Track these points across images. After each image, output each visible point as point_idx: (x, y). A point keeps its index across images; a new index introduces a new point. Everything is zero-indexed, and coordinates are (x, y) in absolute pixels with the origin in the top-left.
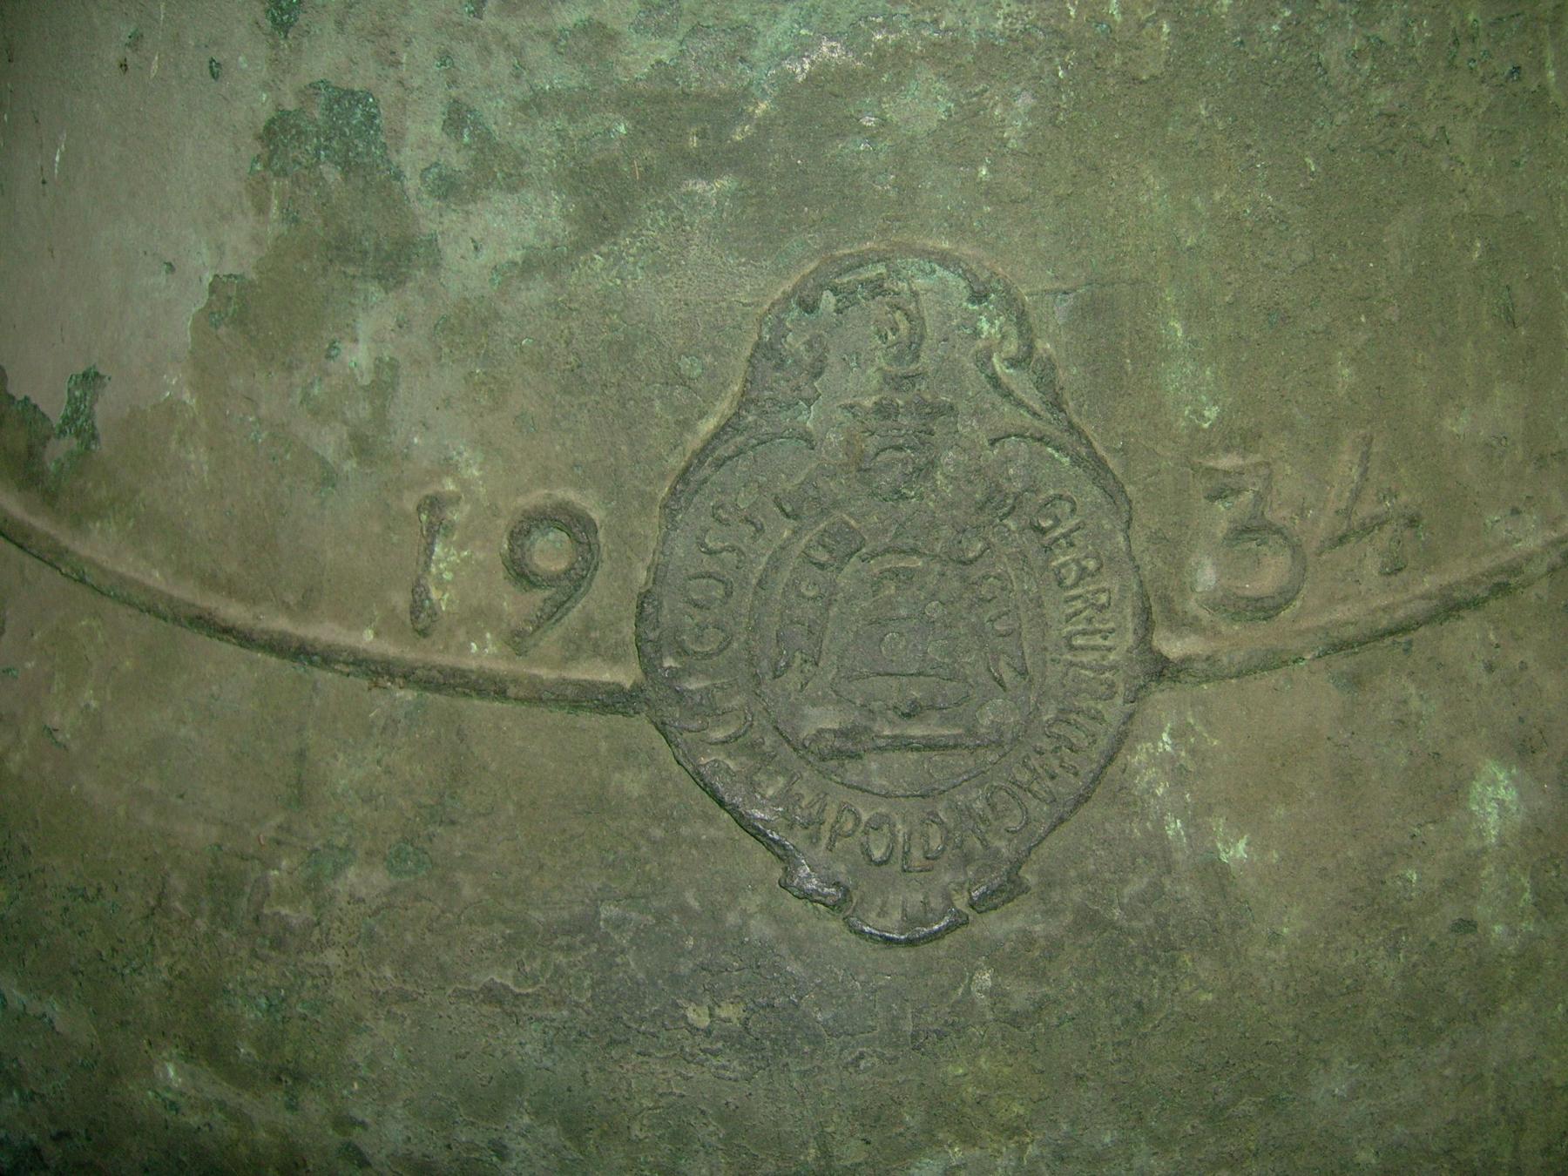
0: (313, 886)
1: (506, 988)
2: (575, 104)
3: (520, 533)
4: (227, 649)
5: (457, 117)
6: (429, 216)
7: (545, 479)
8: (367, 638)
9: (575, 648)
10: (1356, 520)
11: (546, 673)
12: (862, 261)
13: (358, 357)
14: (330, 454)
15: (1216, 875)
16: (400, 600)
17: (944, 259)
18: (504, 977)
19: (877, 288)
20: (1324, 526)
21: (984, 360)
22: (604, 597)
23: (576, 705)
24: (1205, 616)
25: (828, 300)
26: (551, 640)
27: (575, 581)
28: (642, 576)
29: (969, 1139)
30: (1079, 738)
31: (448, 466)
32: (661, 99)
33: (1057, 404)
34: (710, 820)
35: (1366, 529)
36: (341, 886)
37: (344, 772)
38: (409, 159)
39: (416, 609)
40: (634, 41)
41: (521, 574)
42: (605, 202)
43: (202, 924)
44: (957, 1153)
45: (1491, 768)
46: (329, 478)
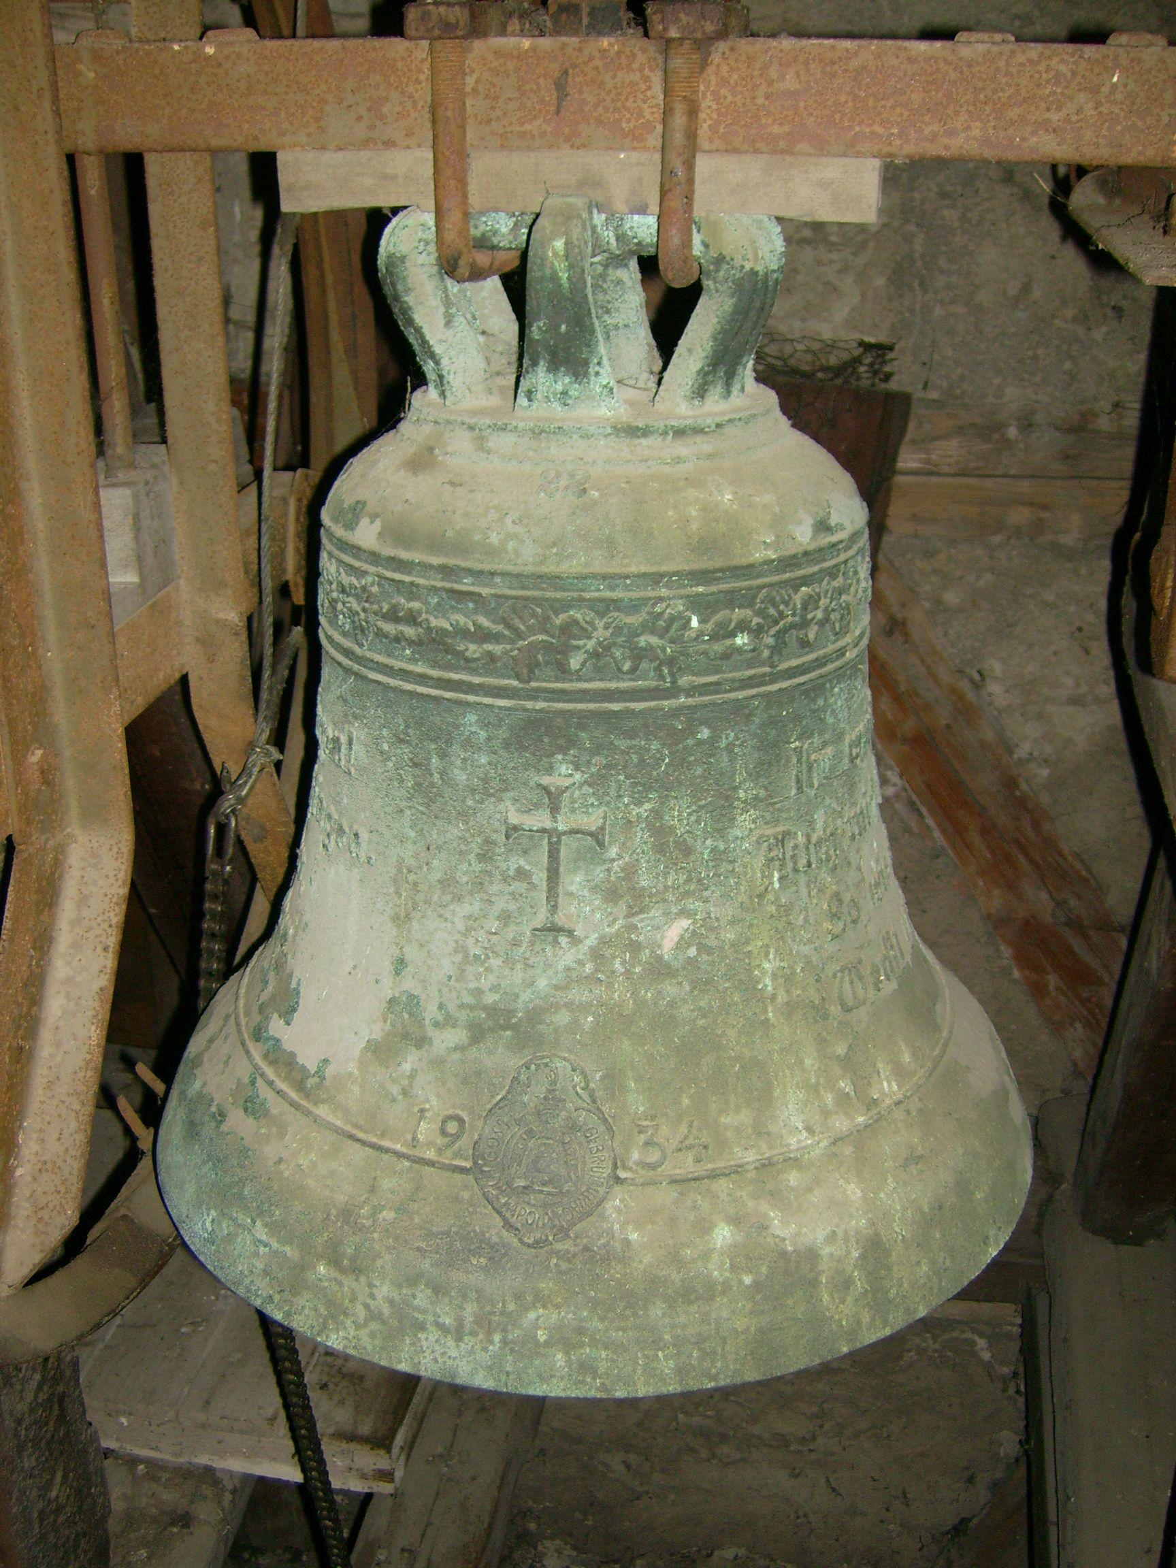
0: (373, 1215)
1: (436, 617)
2: (472, 1008)
3: (444, 1122)
4: (357, 1146)
5: (441, 1006)
6: (431, 1031)
7: (453, 1107)
8: (398, 1147)
9: (457, 1155)
10: (684, 1145)
11: (447, 1162)
12: (543, 1057)
13: (407, 1067)
14: (395, 1093)
15: (627, 1243)
16: (409, 1137)
17: (565, 1059)
18: (423, 1245)
19: (546, 1065)
20: (674, 1144)
21: (574, 1087)
22: (465, 1142)
23: (453, 1171)
24: (634, 1168)
25: (533, 1067)
26: (449, 1153)
27: (457, 1136)
28: (476, 1137)
29: (544, 1307)
30: (591, 1197)
31: (427, 1101)
32: (494, 1009)
33: (594, 1101)
34: (485, 1207)
35: (690, 1148)
36: (381, 1216)
37: (387, 1184)
38: (428, 1016)
39: (414, 1139)
40: (488, 993)
41: (444, 1133)
42: (477, 1033)
43: (339, 1224)
44: (541, 1311)
45: (722, 1225)
46: (394, 1100)
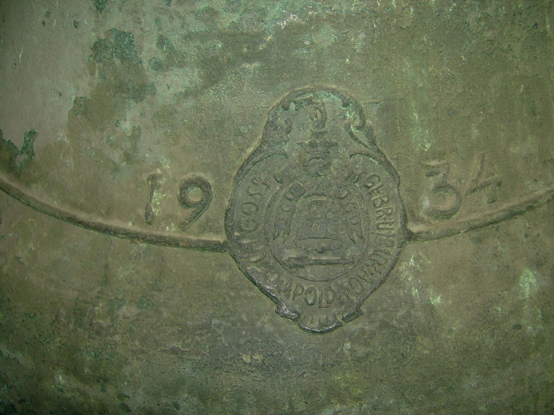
0: (110, 313)
2: (203, 37)
3: (184, 188)
4: (80, 229)
5: (162, 41)
6: (152, 76)
7: (193, 169)
8: (130, 225)
9: (203, 229)
10: (479, 184)
11: (193, 238)
12: (305, 92)
13: (127, 126)
14: (117, 160)
15: (430, 309)
16: (141, 212)
17: (334, 91)
18: (178, 345)
19: (310, 102)
20: (468, 186)
21: (348, 127)
22: (214, 211)
23: (203, 249)
24: (426, 217)
25: (293, 106)
26: (195, 226)
27: (203, 205)
28: (227, 203)
29: (342, 402)
30: (381, 260)
31: (158, 165)
32: (234, 35)
33: (373, 143)
34: (251, 289)
36: (120, 313)
37: (121, 273)
38: (145, 56)
39: (147, 215)
40: (224, 15)
41: (184, 202)
42: (214, 71)
43: (71, 326)
44: (338, 407)
45: (527, 271)
46: (116, 169)
